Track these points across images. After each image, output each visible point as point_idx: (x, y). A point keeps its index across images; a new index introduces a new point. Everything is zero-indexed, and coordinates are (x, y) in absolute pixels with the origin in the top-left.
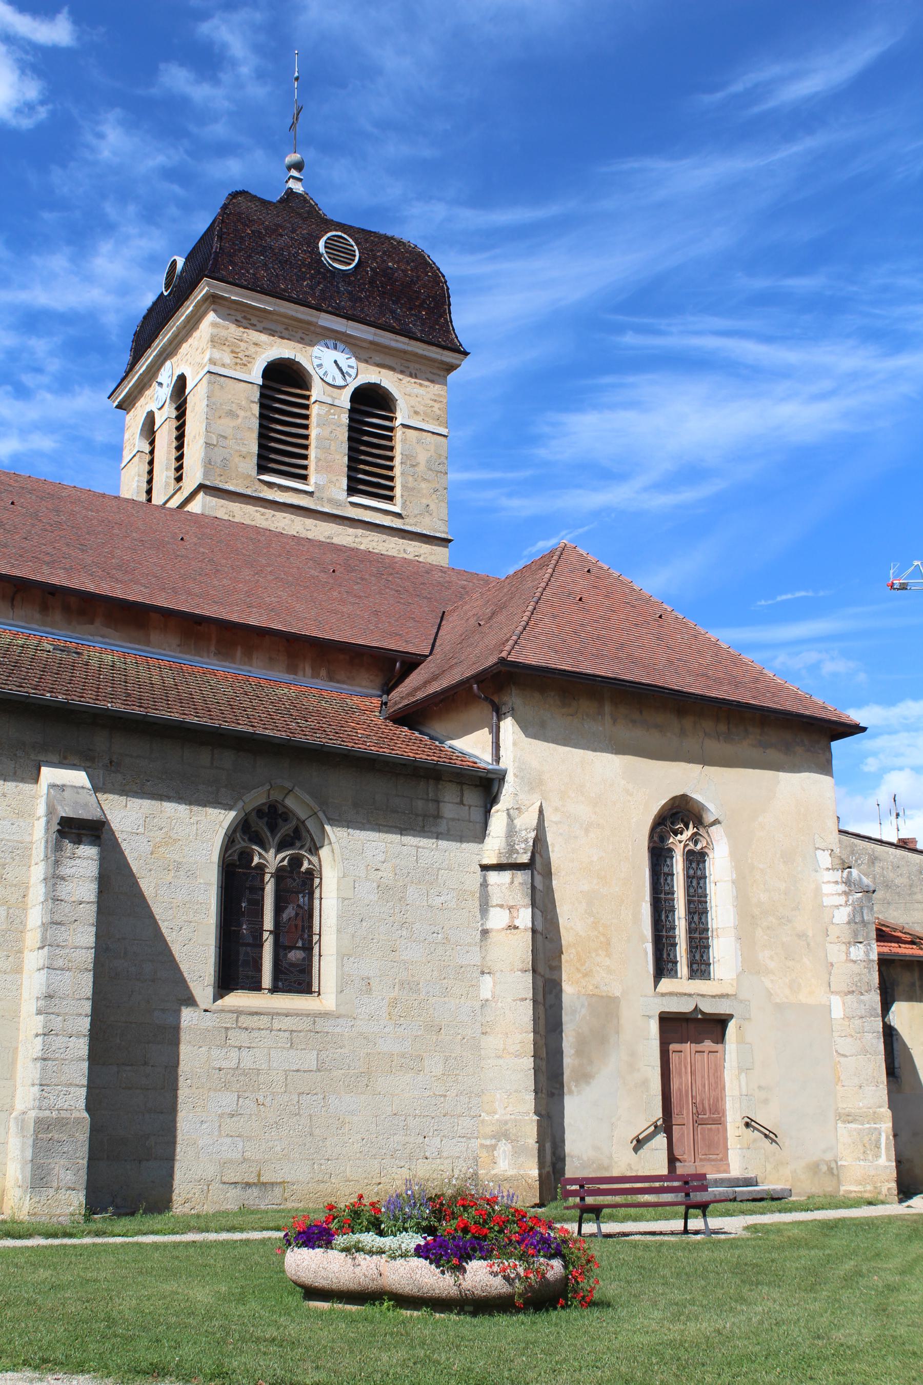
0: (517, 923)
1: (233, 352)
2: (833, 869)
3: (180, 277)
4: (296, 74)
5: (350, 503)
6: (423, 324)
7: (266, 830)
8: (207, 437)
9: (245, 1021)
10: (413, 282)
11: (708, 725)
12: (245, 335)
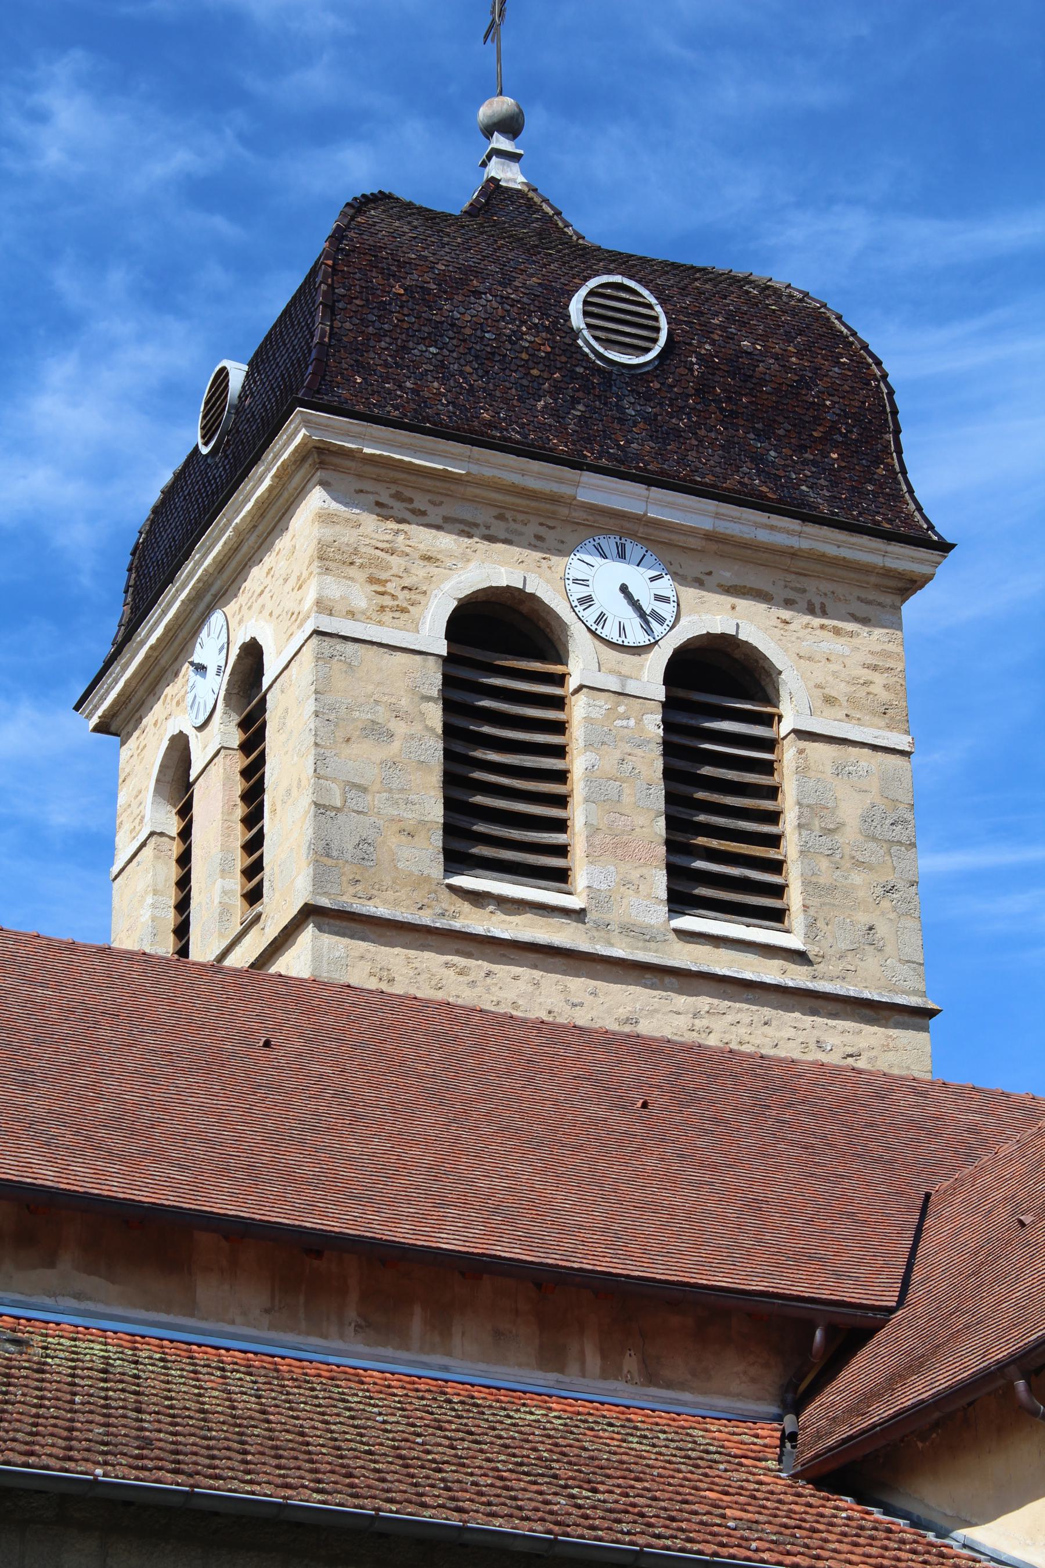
1: (372, 580)
5: (679, 932)
8: (317, 789)
12: (401, 537)
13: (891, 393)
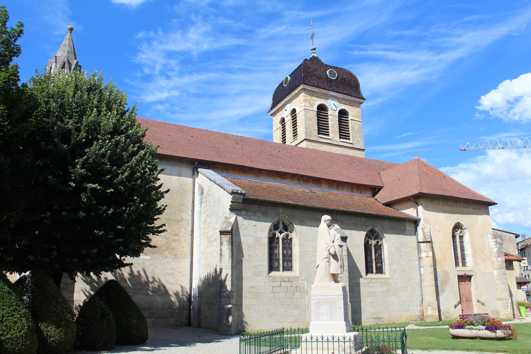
0: (429, 255)
1: (309, 103)
2: (492, 239)
4: (312, 25)
5: (341, 141)
7: (371, 235)
8: (305, 126)
9: (372, 281)
10: (350, 81)
11: (462, 204)
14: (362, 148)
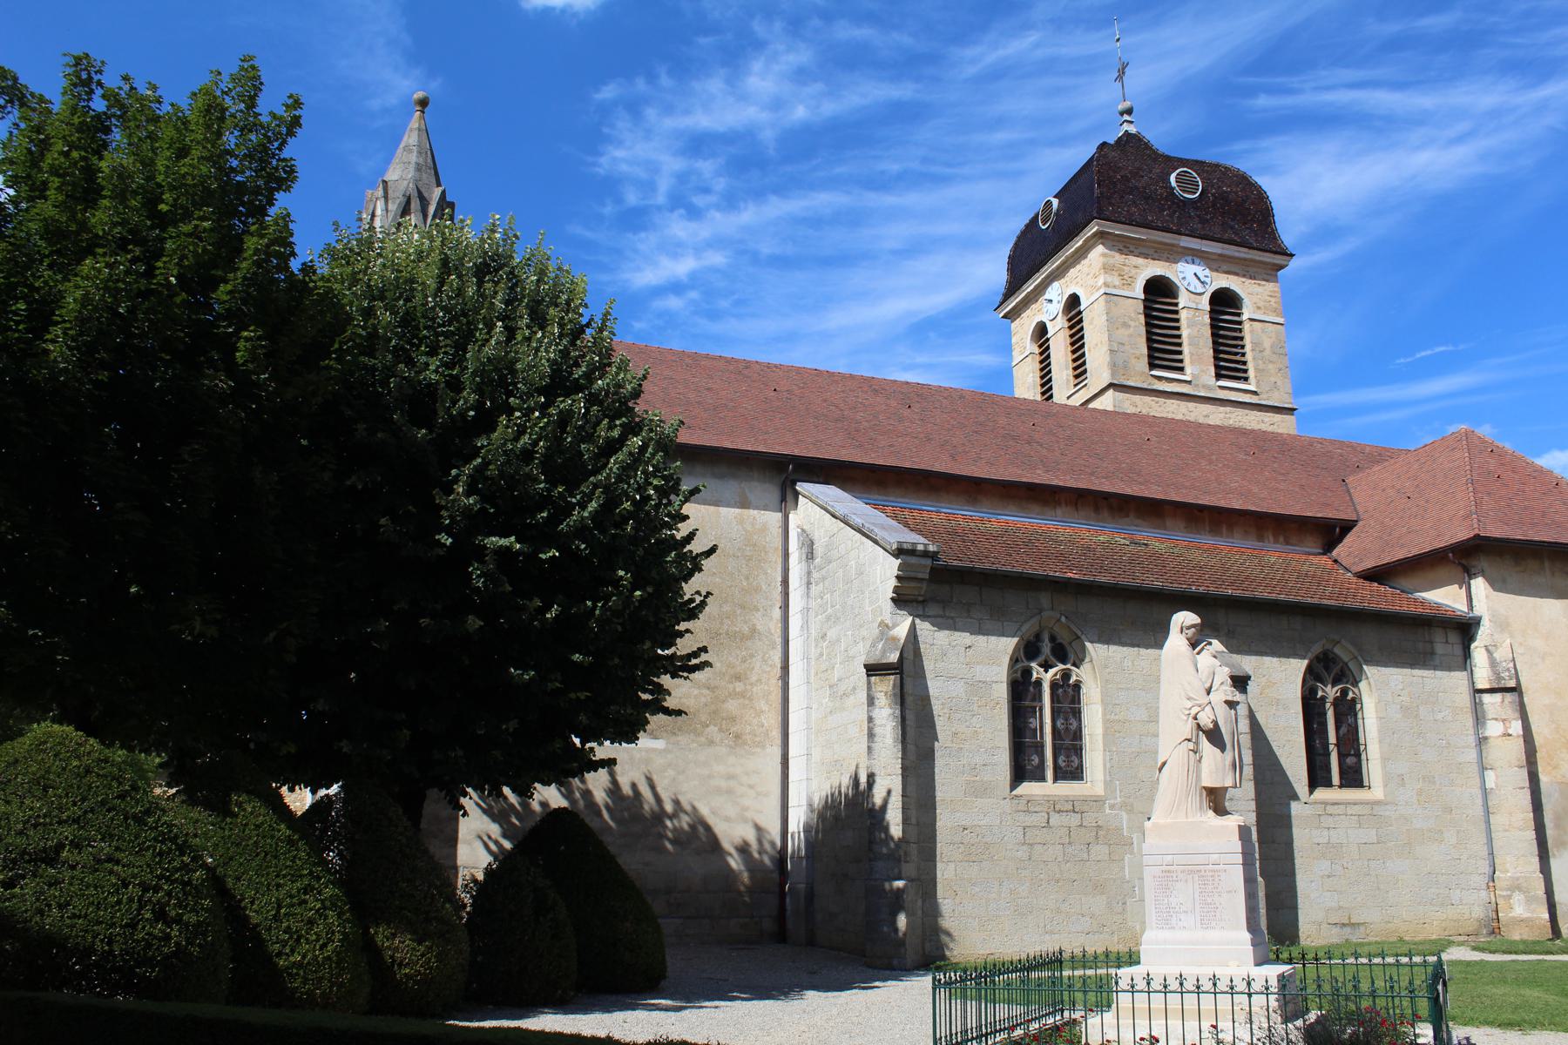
0: (1510, 732)
1: (1120, 275)
3: (1057, 214)
4: (1118, 37)
5: (1219, 387)
6: (1256, 235)
8: (1110, 345)
9: (1330, 809)
13: (1270, 203)
14: (1286, 406)
